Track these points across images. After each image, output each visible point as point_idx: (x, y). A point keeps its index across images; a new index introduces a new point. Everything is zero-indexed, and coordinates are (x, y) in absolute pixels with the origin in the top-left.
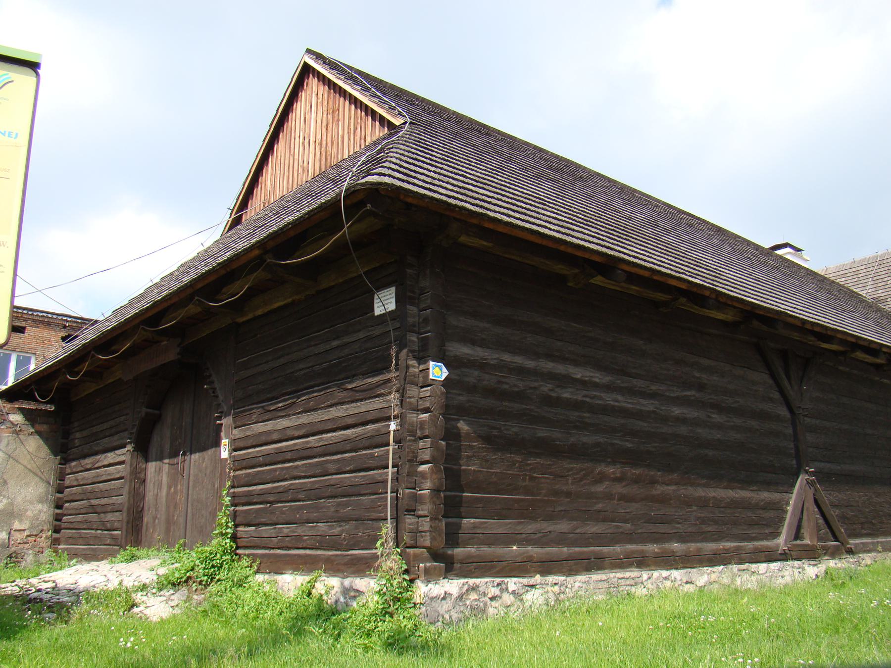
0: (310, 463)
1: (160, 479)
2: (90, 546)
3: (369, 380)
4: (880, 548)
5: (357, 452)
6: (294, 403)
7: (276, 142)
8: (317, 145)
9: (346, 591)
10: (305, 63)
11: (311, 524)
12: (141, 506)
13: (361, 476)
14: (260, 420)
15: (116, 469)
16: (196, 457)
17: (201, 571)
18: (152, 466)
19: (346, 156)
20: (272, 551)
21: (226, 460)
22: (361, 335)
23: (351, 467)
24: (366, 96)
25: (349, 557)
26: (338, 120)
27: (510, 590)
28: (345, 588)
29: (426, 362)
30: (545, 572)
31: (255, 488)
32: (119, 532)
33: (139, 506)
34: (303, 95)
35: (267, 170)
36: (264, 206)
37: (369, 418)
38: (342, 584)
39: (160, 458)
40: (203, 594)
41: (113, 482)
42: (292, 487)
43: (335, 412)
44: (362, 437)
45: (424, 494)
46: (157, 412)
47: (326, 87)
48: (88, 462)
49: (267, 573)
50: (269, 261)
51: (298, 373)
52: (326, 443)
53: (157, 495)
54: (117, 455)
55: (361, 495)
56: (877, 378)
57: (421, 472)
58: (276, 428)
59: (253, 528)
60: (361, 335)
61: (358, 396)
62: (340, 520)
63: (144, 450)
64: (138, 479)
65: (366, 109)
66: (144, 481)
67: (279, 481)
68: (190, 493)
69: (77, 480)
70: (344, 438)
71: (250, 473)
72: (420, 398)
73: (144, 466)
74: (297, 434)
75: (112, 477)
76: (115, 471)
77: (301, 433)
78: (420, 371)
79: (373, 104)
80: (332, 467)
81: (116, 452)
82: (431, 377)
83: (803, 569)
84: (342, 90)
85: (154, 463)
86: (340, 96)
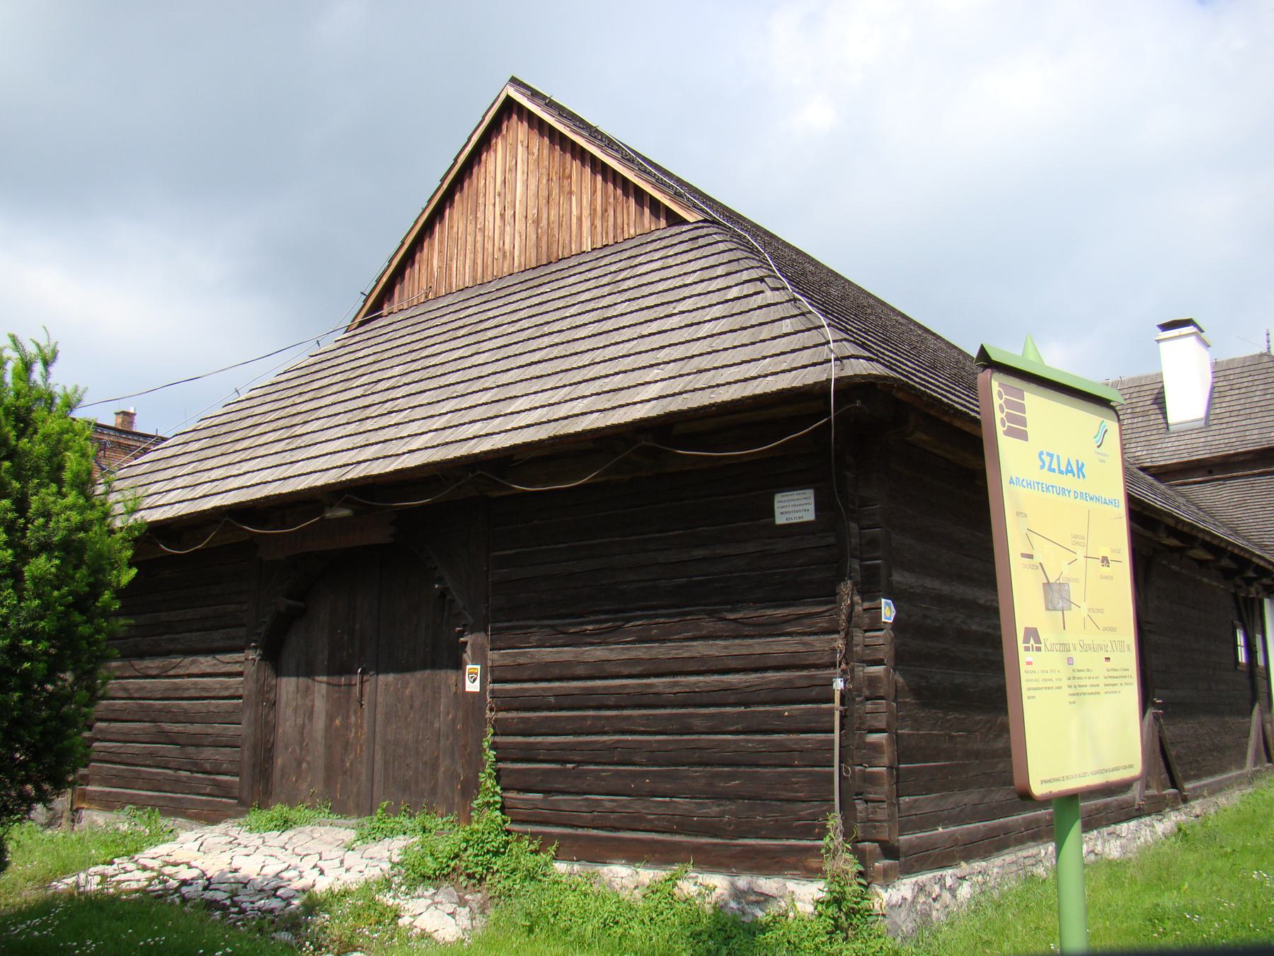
0: (653, 715)
1: (310, 704)
2: (162, 794)
3: (769, 612)
4: (1205, 793)
5: (749, 707)
6: (619, 627)
7: (448, 204)
8: (530, 222)
9: (738, 894)
10: (509, 99)
11: (660, 799)
12: (271, 740)
13: (759, 740)
14: (548, 644)
15: (219, 683)
16: (387, 679)
17: (470, 858)
18: (288, 686)
19: (587, 246)
20: (580, 831)
21: (479, 696)
22: (750, 547)
23: (739, 727)
24: (632, 170)
25: (738, 848)
26: (571, 193)
27: (947, 885)
28: (739, 890)
29: (878, 598)
30: (968, 857)
31: (539, 739)
32: (237, 779)
33: (268, 741)
34: (499, 144)
35: (432, 245)
36: (426, 297)
37: (770, 663)
38: (732, 884)
39: (308, 671)
40: (479, 891)
41: (213, 701)
42: (620, 745)
43: (700, 648)
44: (757, 688)
45: (878, 772)
46: (302, 604)
47: (546, 140)
48: (152, 665)
49: (573, 860)
50: (644, 443)
51: (625, 587)
52: (688, 690)
53: (303, 726)
54: (223, 662)
55: (759, 766)
56: (1199, 577)
57: (871, 744)
58: (581, 659)
59: (539, 796)
60: (750, 547)
61: (746, 630)
62: (719, 797)
63: (274, 659)
64: (267, 700)
65: (625, 184)
66: (274, 704)
67: (588, 734)
68: (377, 729)
69: (126, 690)
70: (724, 686)
71: (529, 718)
72: (866, 646)
73: (274, 682)
74: (626, 671)
75: (212, 694)
76: (219, 686)
77: (638, 670)
78: (864, 610)
79: (644, 182)
80: (697, 723)
81: (218, 657)
82: (883, 620)
83: (1153, 826)
84: (578, 149)
85: (293, 680)
86: (574, 157)
